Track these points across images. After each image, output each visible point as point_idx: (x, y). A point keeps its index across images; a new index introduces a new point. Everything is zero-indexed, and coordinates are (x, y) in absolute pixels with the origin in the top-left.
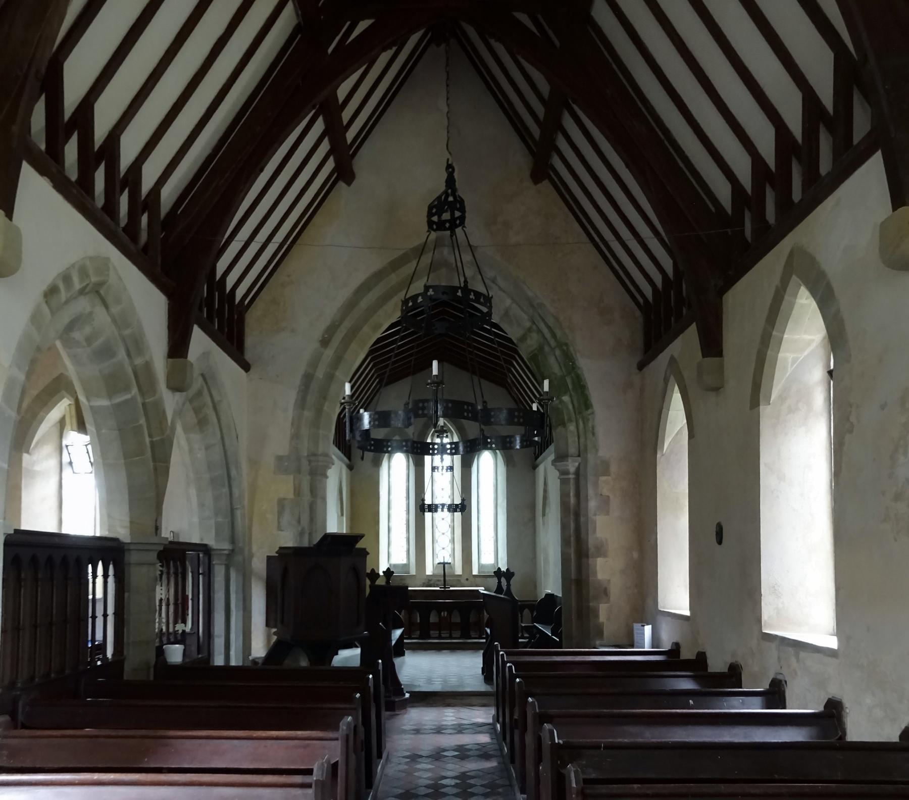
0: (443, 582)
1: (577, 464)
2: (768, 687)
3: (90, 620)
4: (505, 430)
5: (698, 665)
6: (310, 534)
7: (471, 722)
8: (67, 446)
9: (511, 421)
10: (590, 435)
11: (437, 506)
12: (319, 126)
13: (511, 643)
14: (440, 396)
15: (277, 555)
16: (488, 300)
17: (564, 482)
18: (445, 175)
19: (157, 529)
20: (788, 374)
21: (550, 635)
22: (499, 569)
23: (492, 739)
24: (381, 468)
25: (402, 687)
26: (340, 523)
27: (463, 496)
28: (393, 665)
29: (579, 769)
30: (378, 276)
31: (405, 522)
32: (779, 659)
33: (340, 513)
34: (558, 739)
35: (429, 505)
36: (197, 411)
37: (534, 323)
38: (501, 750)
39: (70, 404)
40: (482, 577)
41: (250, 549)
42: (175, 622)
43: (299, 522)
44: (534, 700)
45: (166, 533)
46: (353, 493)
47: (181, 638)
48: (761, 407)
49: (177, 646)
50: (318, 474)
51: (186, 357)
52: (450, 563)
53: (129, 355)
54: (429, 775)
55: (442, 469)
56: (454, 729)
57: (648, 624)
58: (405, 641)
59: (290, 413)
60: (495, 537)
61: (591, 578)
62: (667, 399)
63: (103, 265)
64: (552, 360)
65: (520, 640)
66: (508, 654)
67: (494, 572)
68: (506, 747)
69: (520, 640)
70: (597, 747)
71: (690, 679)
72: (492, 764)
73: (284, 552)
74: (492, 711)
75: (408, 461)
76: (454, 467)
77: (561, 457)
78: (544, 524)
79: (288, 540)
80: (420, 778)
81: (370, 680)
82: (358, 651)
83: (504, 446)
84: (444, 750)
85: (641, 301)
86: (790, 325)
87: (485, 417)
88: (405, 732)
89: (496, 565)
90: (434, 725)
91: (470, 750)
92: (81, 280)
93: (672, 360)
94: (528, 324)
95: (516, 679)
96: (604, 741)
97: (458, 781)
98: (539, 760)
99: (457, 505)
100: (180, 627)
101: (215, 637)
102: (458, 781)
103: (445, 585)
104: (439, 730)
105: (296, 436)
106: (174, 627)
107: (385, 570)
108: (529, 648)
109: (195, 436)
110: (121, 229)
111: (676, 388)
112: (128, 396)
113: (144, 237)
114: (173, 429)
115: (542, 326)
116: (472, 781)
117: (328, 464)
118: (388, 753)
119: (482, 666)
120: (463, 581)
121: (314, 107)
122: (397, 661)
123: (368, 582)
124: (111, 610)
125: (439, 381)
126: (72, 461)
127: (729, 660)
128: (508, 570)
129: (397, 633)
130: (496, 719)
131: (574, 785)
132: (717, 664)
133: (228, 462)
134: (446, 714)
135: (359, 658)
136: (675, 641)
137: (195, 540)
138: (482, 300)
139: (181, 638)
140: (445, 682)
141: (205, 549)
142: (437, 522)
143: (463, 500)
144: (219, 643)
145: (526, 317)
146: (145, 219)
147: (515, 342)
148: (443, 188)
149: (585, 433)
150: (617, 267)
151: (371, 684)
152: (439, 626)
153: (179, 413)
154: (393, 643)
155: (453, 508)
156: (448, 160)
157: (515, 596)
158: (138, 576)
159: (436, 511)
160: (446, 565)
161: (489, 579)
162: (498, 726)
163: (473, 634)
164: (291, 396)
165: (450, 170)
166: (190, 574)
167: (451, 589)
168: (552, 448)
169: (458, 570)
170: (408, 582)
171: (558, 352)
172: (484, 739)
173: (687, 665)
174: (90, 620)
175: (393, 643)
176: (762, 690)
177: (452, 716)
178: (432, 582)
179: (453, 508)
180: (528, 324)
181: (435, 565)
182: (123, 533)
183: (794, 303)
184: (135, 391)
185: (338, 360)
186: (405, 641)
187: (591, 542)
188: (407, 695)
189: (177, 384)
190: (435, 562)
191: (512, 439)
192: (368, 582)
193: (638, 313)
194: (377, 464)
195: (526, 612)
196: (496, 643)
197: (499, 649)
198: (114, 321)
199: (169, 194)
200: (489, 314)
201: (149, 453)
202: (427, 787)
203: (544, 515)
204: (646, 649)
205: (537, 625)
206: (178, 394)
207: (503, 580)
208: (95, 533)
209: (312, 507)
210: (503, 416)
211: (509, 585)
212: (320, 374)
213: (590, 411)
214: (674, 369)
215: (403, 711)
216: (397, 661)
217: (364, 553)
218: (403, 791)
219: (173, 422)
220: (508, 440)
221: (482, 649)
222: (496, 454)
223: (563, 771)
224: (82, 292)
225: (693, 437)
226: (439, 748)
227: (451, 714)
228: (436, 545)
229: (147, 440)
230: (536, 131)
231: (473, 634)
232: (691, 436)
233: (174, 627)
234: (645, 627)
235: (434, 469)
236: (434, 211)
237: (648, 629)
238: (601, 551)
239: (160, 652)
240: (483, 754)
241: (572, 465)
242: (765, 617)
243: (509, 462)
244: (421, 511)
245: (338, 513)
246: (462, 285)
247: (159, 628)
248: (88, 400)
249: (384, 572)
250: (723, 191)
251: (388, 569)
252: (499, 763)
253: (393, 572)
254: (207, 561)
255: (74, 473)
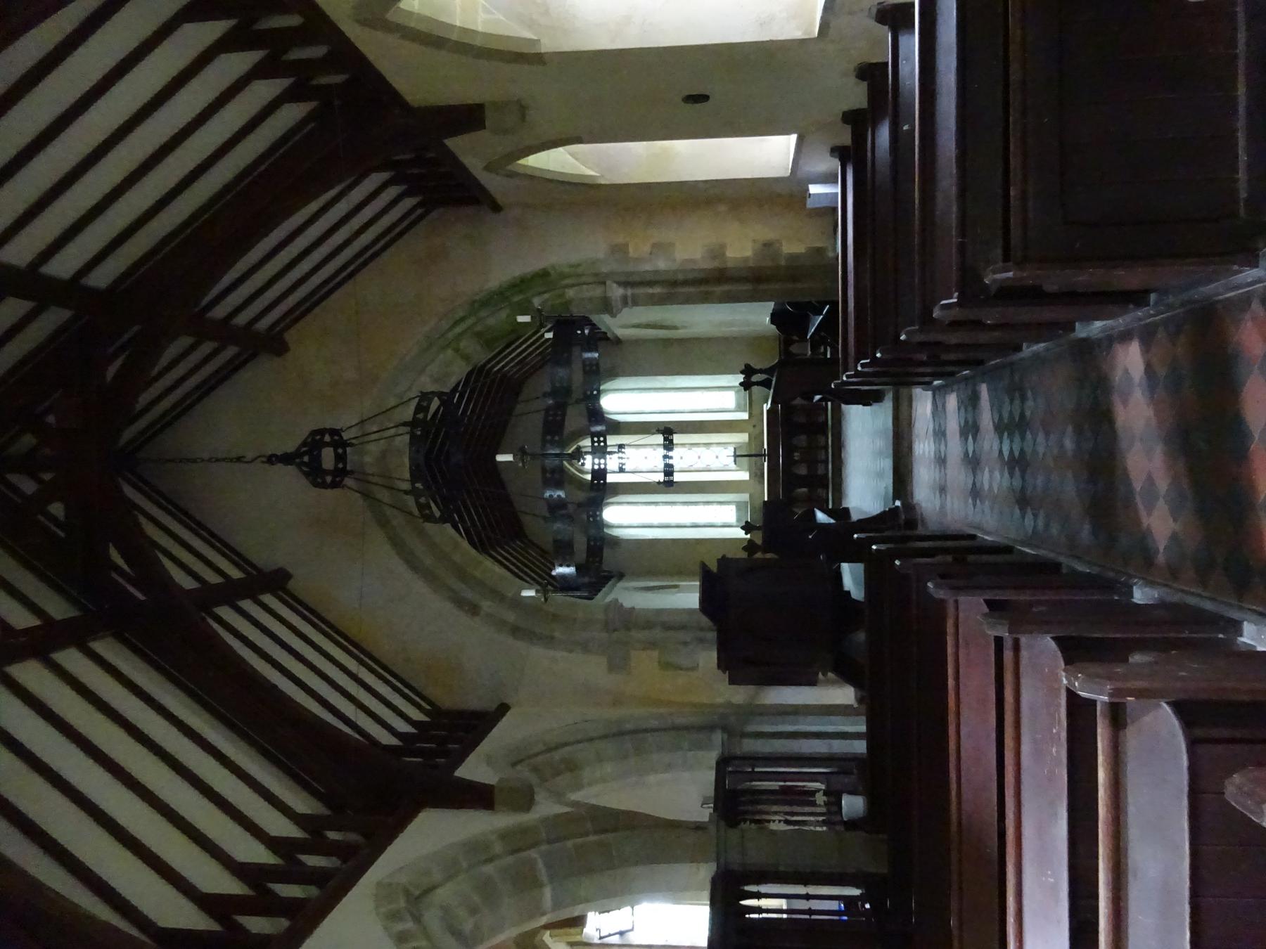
0: (758, 458)
1: (615, 285)
2: (886, 27)
3: (814, 917)
4: (577, 367)
5: (858, 121)
6: (702, 629)
7: (931, 419)
8: (601, 938)
9: (568, 363)
10: (580, 270)
11: (667, 465)
12: (225, 612)
13: (833, 368)
14: (538, 450)
15: (727, 672)
16: (425, 397)
17: (635, 302)
18: (280, 465)
19: (699, 827)
20: (502, 18)
21: (822, 317)
22: (741, 384)
23: (952, 391)
24: (621, 538)
25: (887, 509)
26: (689, 590)
27: (655, 431)
28: (860, 521)
29: (991, 268)
30: (397, 544)
31: (685, 507)
32: (851, 13)
33: (674, 590)
34: (952, 298)
35: (665, 475)
36: (558, 773)
37: (448, 346)
38: (966, 378)
39: (551, 936)
40: (752, 407)
41: (720, 706)
42: (814, 804)
43: (685, 644)
44: (903, 333)
45: (704, 814)
46: (651, 573)
47: (834, 797)
48: (543, 51)
49: (843, 802)
50: (628, 620)
51: (492, 786)
52: (735, 449)
53: (490, 860)
54: (997, 474)
55: (622, 458)
56: (940, 440)
57: (808, 190)
58: (830, 507)
59: (559, 654)
60: (703, 390)
61: (751, 264)
62: (537, 174)
63: (385, 891)
64: (491, 321)
65: (829, 356)
66: (846, 370)
67: (745, 390)
68: (962, 372)
69: (829, 356)
70: (962, 248)
71: (876, 131)
72: (984, 389)
73: (723, 664)
74: (918, 391)
75: (612, 503)
76: (619, 443)
77: (607, 306)
78: (684, 327)
79: (709, 657)
80: (1000, 486)
81: (880, 548)
82: (845, 567)
83: (597, 376)
84: (966, 453)
85: (419, 211)
86: (444, 19)
87: (562, 395)
88: (943, 507)
89: (736, 389)
90: (935, 467)
91: (966, 422)
92: (401, 919)
93: (487, 168)
94: (450, 352)
95: (877, 357)
96: (955, 240)
97: (1006, 434)
98: (978, 325)
99: (665, 439)
100: (820, 799)
101: (831, 752)
102: (1006, 434)
103: (760, 455)
104: (941, 461)
105: (585, 647)
106: (820, 806)
107: (744, 532)
108: (838, 345)
109: (586, 774)
110: (344, 866)
111: (522, 162)
112: (540, 864)
113: (353, 837)
114: (576, 804)
115: (450, 335)
116: (1006, 415)
117: (616, 605)
118: (971, 527)
119: (861, 406)
120: (757, 430)
121: (204, 619)
122: (855, 517)
123: (759, 555)
124: (801, 890)
125: (521, 453)
126: (618, 931)
127: (853, 80)
128: (742, 372)
129: (821, 517)
130: (927, 385)
131: (1010, 274)
132: (857, 96)
133: (618, 733)
134: (921, 452)
135: (851, 564)
136: (829, 154)
137: (712, 776)
138: (425, 404)
139: (834, 797)
140: (880, 453)
141: (723, 764)
142: (684, 465)
143: (659, 431)
144: (839, 747)
145: (441, 356)
146: (332, 835)
147: (470, 369)
148: (291, 469)
149: (579, 276)
150: (382, 243)
151: (883, 547)
152: (812, 463)
153: (558, 796)
154: (832, 521)
155: (669, 445)
156: (263, 462)
157: (773, 364)
158: (757, 854)
159: (672, 466)
160: (738, 454)
161: (754, 397)
162: (936, 383)
163: (822, 419)
164: (538, 653)
165: (274, 459)
166: (754, 783)
167: (766, 447)
168: (595, 318)
169: (743, 438)
170: (759, 503)
171: (483, 314)
172: (952, 401)
173: (859, 138)
174: (814, 917)
175: (832, 521)
176: (890, 35)
177: (924, 445)
178: (759, 474)
179: (669, 445)
180: (450, 352)
181: (738, 468)
182: (706, 872)
183: (418, 14)
184: (533, 854)
185: (496, 595)
186: (830, 507)
187: (709, 265)
188: (898, 503)
189: (523, 799)
190: (733, 469)
191: (588, 363)
192: (759, 555)
193: (434, 214)
194: (616, 542)
195: (794, 349)
196: (833, 386)
197: (839, 381)
198: (449, 878)
199: (302, 803)
200: (440, 395)
201: (609, 837)
202: (1011, 475)
203: (675, 328)
204: (839, 190)
205: (810, 334)
206: (537, 798)
207: (755, 378)
208: (706, 905)
209: (668, 627)
210: (561, 372)
211: (761, 371)
212: (511, 617)
213: (552, 272)
214: (503, 163)
215: (917, 507)
216: (855, 517)
217: (724, 561)
218: (1017, 507)
219: (567, 805)
220: (548, 475)
221: (840, 406)
222: (606, 391)
223: (993, 290)
224: (417, 919)
225: (580, 137)
226: (963, 460)
227: (922, 446)
228: (713, 467)
229: (592, 838)
230: (231, 351)
231: (822, 419)
232: (579, 140)
233: (820, 806)
234: (811, 193)
235: (621, 470)
236: (319, 480)
237: (814, 189)
238: (717, 252)
239: (852, 825)
240: (971, 402)
241: (617, 292)
242: (798, 34)
243: (613, 374)
244: (672, 486)
245: (676, 593)
246: (408, 429)
247: (821, 826)
248: (543, 914)
249: (746, 534)
250: (291, 114)
251: (743, 528)
252: (983, 382)
253: (747, 522)
254: (736, 762)
255: (632, 930)
